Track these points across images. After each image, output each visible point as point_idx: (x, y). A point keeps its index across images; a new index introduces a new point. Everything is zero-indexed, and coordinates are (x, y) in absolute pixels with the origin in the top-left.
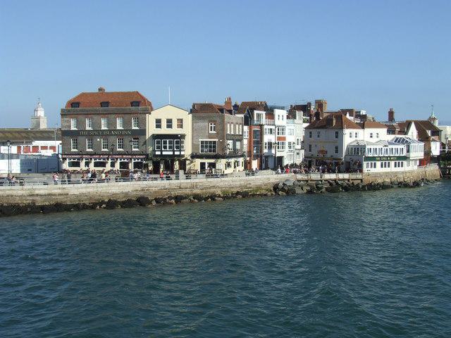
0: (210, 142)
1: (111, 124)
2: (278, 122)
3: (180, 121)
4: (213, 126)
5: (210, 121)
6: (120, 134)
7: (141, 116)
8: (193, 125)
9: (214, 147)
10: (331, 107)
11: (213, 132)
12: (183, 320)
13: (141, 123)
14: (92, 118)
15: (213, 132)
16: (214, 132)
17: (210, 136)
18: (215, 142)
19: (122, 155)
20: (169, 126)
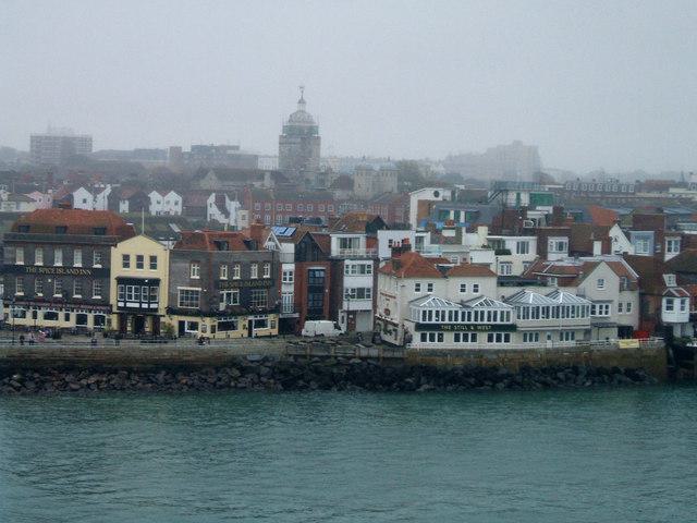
3: (153, 259)
13: (106, 260)
20: (140, 266)
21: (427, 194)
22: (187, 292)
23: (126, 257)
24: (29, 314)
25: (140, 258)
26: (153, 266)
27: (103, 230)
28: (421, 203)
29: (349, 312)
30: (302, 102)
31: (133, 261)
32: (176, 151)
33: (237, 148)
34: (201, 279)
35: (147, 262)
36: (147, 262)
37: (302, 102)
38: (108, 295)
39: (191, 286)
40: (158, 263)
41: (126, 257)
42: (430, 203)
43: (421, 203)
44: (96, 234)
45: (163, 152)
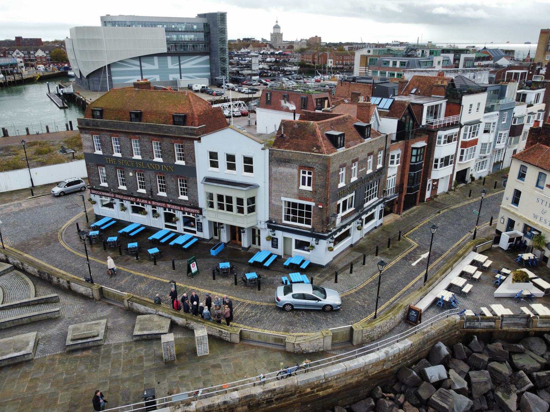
0: (301, 206)
1: (126, 150)
2: (465, 117)
3: (248, 160)
4: (307, 175)
5: (301, 167)
6: (157, 168)
7: (187, 144)
8: (270, 170)
9: (309, 215)
10: (283, 379)
11: (306, 188)
12: (502, 154)
13: (189, 156)
14: (117, 136)
15: (306, 188)
16: (310, 189)
17: (302, 195)
18: (309, 207)
19: (166, 203)
20: (231, 167)
21: (364, 52)
22: (294, 205)
23: (213, 155)
24: (117, 205)
25: (231, 158)
26: (249, 169)
27: (183, 119)
28: (362, 57)
29: (434, 181)
30: (277, 22)
31: (222, 161)
32: (239, 40)
33: (254, 39)
34: (314, 192)
35: (240, 163)
36: (240, 163)
37: (277, 22)
38: (196, 196)
39: (300, 198)
40: (255, 165)
41: (213, 155)
42: (367, 57)
43: (362, 57)
44: (174, 123)
45: (236, 41)
